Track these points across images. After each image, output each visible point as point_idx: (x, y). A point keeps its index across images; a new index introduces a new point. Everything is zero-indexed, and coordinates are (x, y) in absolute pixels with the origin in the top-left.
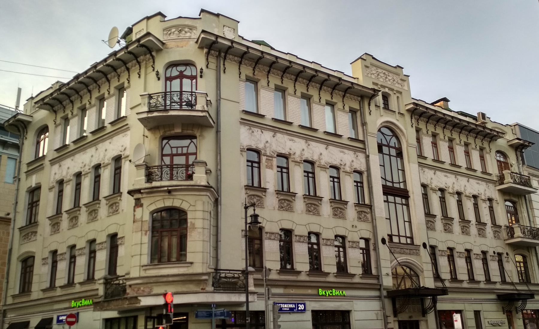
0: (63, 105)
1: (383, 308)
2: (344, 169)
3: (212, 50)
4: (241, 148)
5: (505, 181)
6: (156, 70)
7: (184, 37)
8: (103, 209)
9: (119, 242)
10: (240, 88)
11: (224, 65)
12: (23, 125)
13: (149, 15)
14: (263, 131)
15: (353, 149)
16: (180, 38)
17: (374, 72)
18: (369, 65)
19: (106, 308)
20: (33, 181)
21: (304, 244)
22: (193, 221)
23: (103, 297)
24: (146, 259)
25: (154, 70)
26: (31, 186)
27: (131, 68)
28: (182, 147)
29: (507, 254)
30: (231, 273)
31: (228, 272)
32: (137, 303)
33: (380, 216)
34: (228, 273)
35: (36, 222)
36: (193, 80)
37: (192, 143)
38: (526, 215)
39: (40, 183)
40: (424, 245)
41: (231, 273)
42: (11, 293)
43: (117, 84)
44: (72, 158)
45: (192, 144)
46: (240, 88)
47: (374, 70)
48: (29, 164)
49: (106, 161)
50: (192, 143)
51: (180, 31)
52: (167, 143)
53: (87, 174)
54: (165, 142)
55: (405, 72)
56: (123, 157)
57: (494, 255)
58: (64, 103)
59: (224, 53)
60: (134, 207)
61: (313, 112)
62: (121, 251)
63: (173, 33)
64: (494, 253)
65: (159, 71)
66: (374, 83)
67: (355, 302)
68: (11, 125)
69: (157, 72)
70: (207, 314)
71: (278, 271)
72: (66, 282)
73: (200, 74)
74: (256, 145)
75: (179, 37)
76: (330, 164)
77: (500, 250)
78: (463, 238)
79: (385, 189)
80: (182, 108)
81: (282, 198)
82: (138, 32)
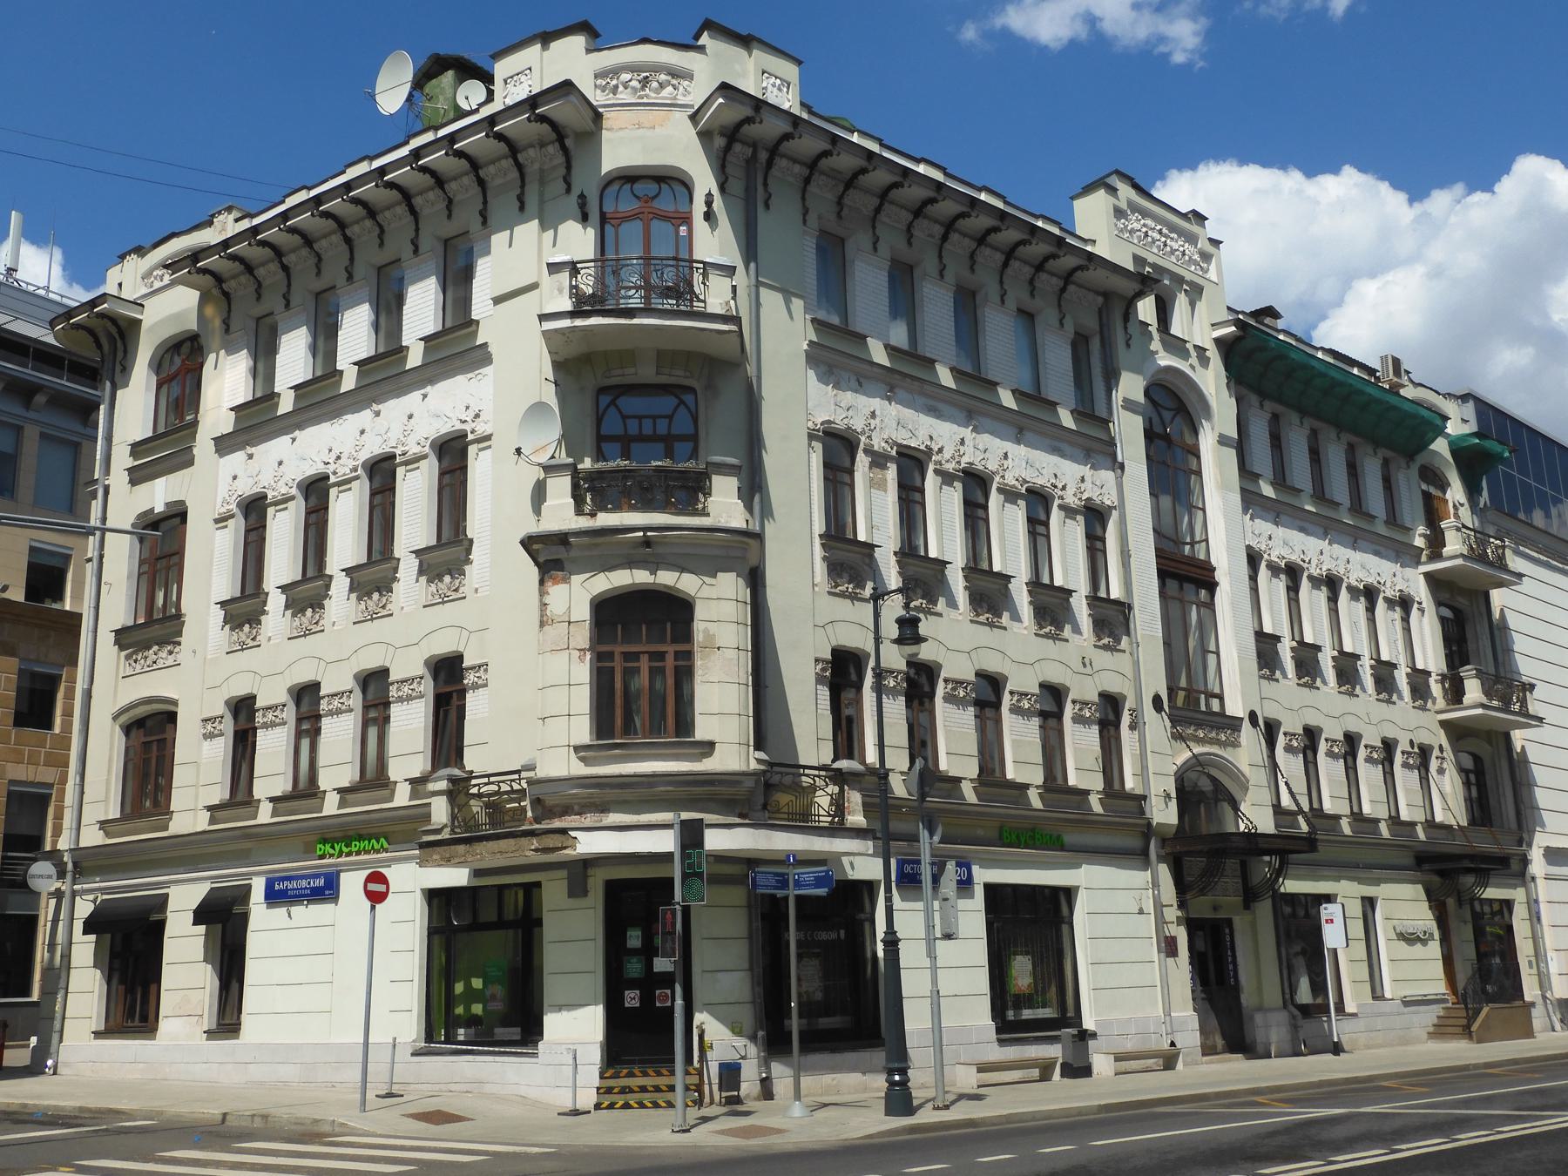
0: (255, 277)
1: (1155, 884)
2: (1061, 498)
5: (1445, 549)
6: (576, 192)
7: (656, 98)
8: (408, 584)
9: (470, 678)
10: (806, 253)
11: (765, 184)
12: (114, 330)
14: (861, 380)
16: (645, 100)
17: (1136, 226)
19: (462, 859)
20: (158, 494)
22: (712, 627)
23: (448, 830)
24: (582, 731)
25: (568, 190)
26: (152, 510)
28: (654, 418)
29: (1441, 749)
30: (493, 783)
31: (486, 780)
32: (565, 848)
33: (1148, 632)
34: (486, 784)
35: (167, 618)
36: (680, 225)
37: (682, 406)
38: (1488, 644)
39: (182, 503)
40: (1253, 717)
41: (493, 783)
42: (92, 814)
45: (682, 410)
46: (806, 253)
47: (1135, 223)
48: (137, 449)
49: (414, 449)
50: (682, 406)
51: (645, 82)
52: (613, 403)
53: (349, 481)
55: (1211, 229)
56: (470, 437)
57: (1410, 750)
59: (767, 150)
60: (542, 582)
61: (985, 330)
62: (475, 704)
64: (1411, 742)
66: (1137, 259)
68: (78, 329)
69: (582, 196)
70: (777, 881)
72: (289, 787)
74: (846, 421)
75: (641, 97)
76: (1028, 482)
77: (1423, 738)
78: (1342, 703)
79: (1163, 561)
80: (650, 304)
82: (512, 77)
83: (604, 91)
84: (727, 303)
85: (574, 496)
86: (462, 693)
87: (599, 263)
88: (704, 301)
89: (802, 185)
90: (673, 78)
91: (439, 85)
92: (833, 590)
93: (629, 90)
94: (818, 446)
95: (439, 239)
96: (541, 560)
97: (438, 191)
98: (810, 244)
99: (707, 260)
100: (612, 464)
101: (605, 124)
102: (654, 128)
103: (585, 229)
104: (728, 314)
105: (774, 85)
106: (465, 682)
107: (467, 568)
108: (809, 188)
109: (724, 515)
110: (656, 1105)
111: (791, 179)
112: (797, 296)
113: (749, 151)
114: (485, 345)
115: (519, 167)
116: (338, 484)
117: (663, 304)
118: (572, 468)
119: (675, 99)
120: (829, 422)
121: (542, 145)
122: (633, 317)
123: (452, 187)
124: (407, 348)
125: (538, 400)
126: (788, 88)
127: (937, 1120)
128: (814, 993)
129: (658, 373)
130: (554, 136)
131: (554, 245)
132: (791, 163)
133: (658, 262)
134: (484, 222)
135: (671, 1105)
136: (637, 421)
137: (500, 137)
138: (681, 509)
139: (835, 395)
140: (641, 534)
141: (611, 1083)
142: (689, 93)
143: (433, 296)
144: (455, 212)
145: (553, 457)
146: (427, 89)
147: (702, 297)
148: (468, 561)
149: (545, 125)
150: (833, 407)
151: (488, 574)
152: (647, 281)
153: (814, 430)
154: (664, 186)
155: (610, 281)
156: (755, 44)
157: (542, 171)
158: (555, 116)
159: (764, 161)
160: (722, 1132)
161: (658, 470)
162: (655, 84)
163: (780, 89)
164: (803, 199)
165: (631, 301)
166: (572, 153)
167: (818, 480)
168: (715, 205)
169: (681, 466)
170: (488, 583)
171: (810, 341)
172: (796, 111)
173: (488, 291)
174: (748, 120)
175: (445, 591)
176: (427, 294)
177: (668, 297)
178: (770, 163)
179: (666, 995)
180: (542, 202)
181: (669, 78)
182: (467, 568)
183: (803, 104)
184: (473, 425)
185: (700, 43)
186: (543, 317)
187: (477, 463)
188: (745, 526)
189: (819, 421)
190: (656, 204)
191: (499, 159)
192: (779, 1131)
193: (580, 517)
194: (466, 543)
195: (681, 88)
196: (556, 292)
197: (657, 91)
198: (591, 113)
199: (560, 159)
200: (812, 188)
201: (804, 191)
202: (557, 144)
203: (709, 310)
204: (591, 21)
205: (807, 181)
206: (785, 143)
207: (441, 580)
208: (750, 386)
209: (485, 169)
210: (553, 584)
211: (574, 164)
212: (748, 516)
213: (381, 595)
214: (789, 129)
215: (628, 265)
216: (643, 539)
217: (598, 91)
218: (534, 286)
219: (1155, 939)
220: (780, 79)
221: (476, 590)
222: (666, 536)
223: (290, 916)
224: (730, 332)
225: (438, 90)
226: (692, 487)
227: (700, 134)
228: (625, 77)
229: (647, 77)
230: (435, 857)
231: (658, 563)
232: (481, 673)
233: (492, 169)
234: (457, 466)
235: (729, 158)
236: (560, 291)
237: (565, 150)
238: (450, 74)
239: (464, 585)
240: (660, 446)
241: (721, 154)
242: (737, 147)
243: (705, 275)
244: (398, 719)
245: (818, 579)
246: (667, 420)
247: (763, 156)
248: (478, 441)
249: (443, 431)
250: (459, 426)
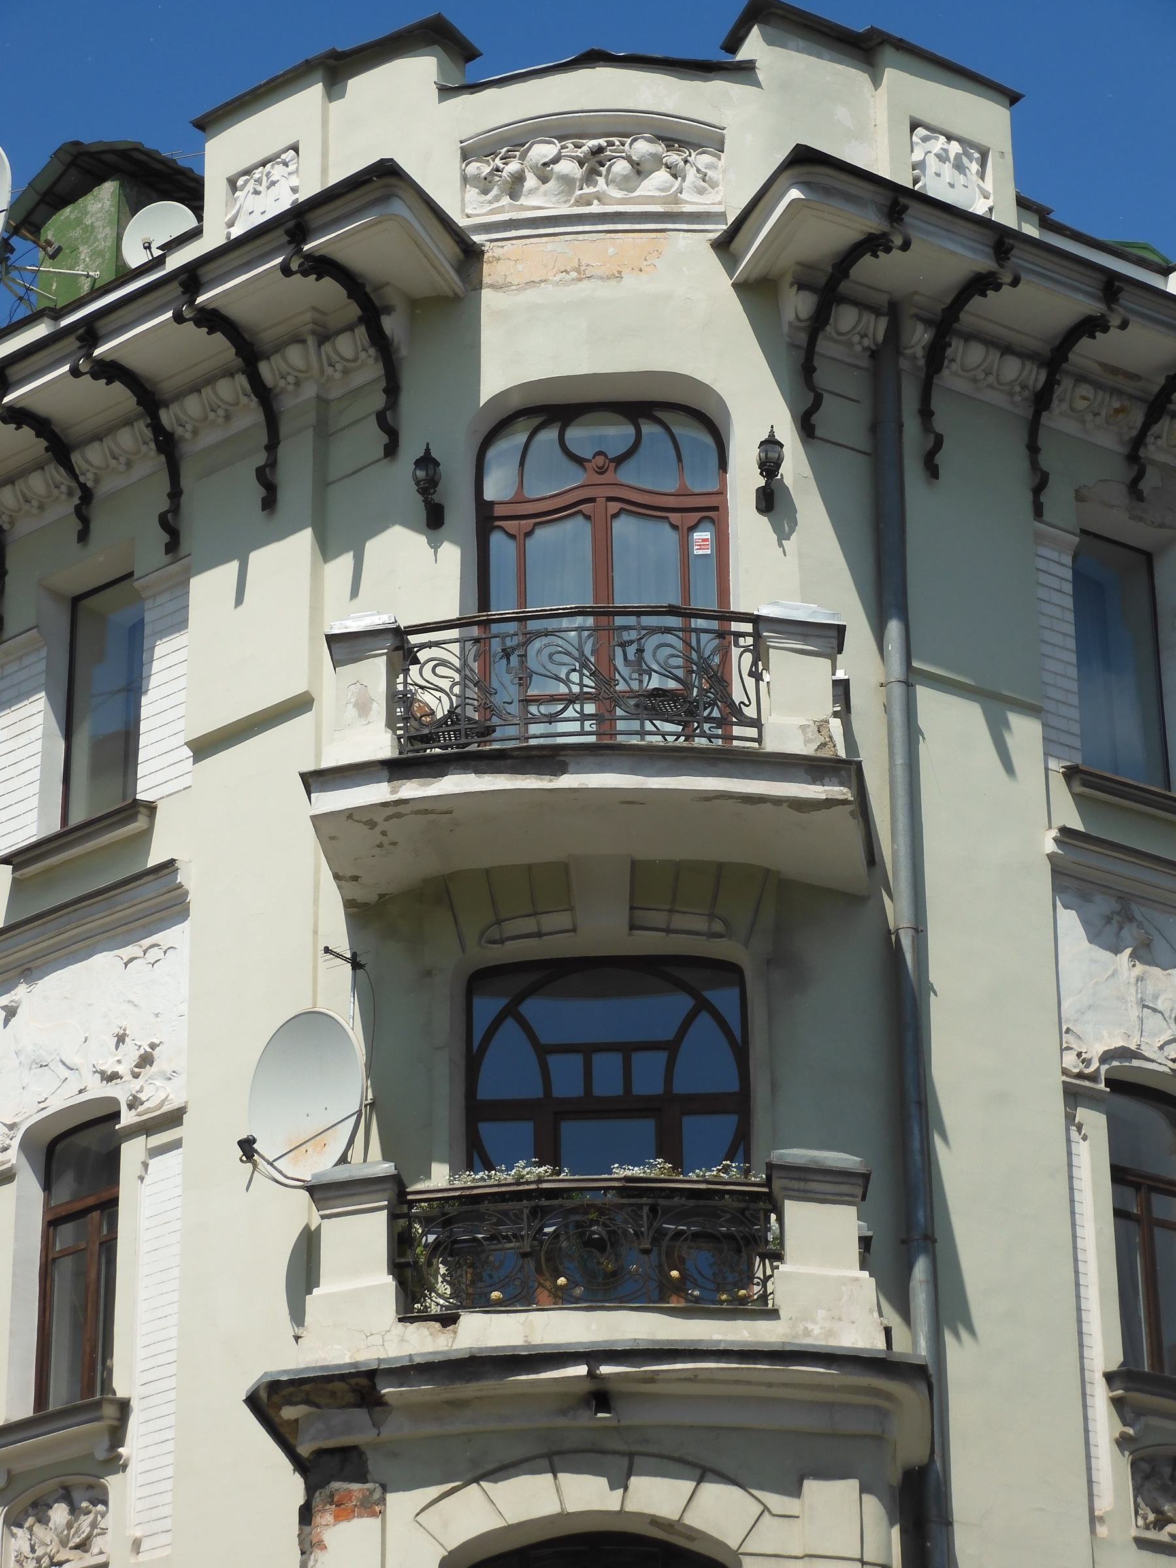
3: (844, 300)
4: (1065, 1072)
6: (411, 450)
11: (926, 413)
13: (344, 45)
16: (596, 208)
25: (391, 449)
28: (627, 1049)
36: (693, 528)
51: (595, 162)
52: (510, 1011)
54: (487, 1007)
56: (127, 1118)
59: (928, 322)
60: (306, 1515)
63: (544, 172)
65: (434, 454)
69: (427, 461)
73: (762, 482)
82: (248, 172)
83: (485, 192)
84: (821, 726)
85: (398, 1267)
87: (475, 631)
88: (757, 723)
89: (1029, 413)
90: (669, 147)
91: (79, 221)
92: (1151, 1535)
93: (552, 184)
94: (1094, 1121)
95: (55, 595)
96: (304, 1450)
97: (56, 473)
98: (1055, 569)
99: (765, 611)
100: (501, 1177)
101: (490, 273)
102: (619, 276)
103: (435, 545)
104: (826, 753)
105: (942, 157)
107: (112, 1482)
108: (1045, 419)
109: (821, 1314)
111: (997, 398)
112: (1032, 710)
113: (881, 326)
114: (169, 865)
115: (264, 395)
117: (643, 733)
118: (391, 1190)
119: (677, 201)
120: (1124, 1053)
121: (324, 336)
122: (560, 769)
123: (89, 459)
125: (306, 1006)
126: (983, 164)
129: (633, 927)
130: (354, 310)
131: (355, 593)
132: (995, 355)
133: (631, 620)
134: (173, 546)
136: (577, 1060)
137: (211, 319)
138: (697, 1300)
139: (1140, 979)
140: (582, 1370)
142: (714, 185)
143: (38, 746)
144: (97, 527)
145: (343, 1160)
146: (49, 233)
147: (750, 712)
148: (115, 1464)
149: (328, 281)
150: (1134, 1012)
151: (168, 1498)
152: (605, 680)
153: (1080, 1076)
154: (649, 429)
155: (506, 690)
156: (888, 53)
157: (322, 401)
158: (354, 257)
159: (920, 353)
161: (631, 1189)
162: (621, 167)
163: (959, 167)
164: (1033, 449)
165: (562, 727)
166: (404, 352)
167: (1096, 1216)
168: (788, 472)
169: (696, 1177)
170: (167, 1524)
171: (1064, 830)
172: (1008, 216)
173: (181, 725)
174: (873, 244)
175: (52, 1549)
176: (23, 740)
177: (655, 714)
178: (936, 357)
180: (322, 484)
181: (660, 148)
182: (112, 1482)
183: (1023, 203)
184: (136, 1085)
185: (743, 55)
186: (315, 780)
187: (145, 1189)
188: (881, 1344)
189: (1095, 1050)
190: (627, 475)
191: (210, 380)
193: (412, 1328)
194: (109, 1411)
195: (691, 173)
196: (351, 712)
197: (625, 183)
198: (452, 249)
199: (371, 370)
200: (1056, 420)
201: (1034, 428)
202: (361, 331)
203: (772, 745)
205: (1042, 400)
206: (976, 302)
207: (43, 1520)
208: (896, 952)
209: (175, 408)
210: (338, 1518)
212: (893, 1318)
213: (74, 1510)
214: (983, 262)
215: (547, 634)
216: (588, 1386)
217: (472, 193)
218: (300, 705)
220: (960, 140)
221: (137, 1545)
222: (652, 1378)
224: (829, 803)
225: (77, 232)
226: (730, 1237)
227: (741, 287)
228: (542, 151)
229: (600, 150)
231: (631, 1455)
233: (192, 406)
234: (90, 1201)
235: (823, 346)
236: (363, 708)
237: (381, 343)
238: (108, 191)
239: (104, 1531)
240: (645, 1128)
241: (803, 338)
242: (846, 318)
243: (759, 653)
245: (1104, 1504)
246: (662, 1057)
247: (919, 337)
248: (147, 1128)
249: (57, 1104)
250: (98, 1090)
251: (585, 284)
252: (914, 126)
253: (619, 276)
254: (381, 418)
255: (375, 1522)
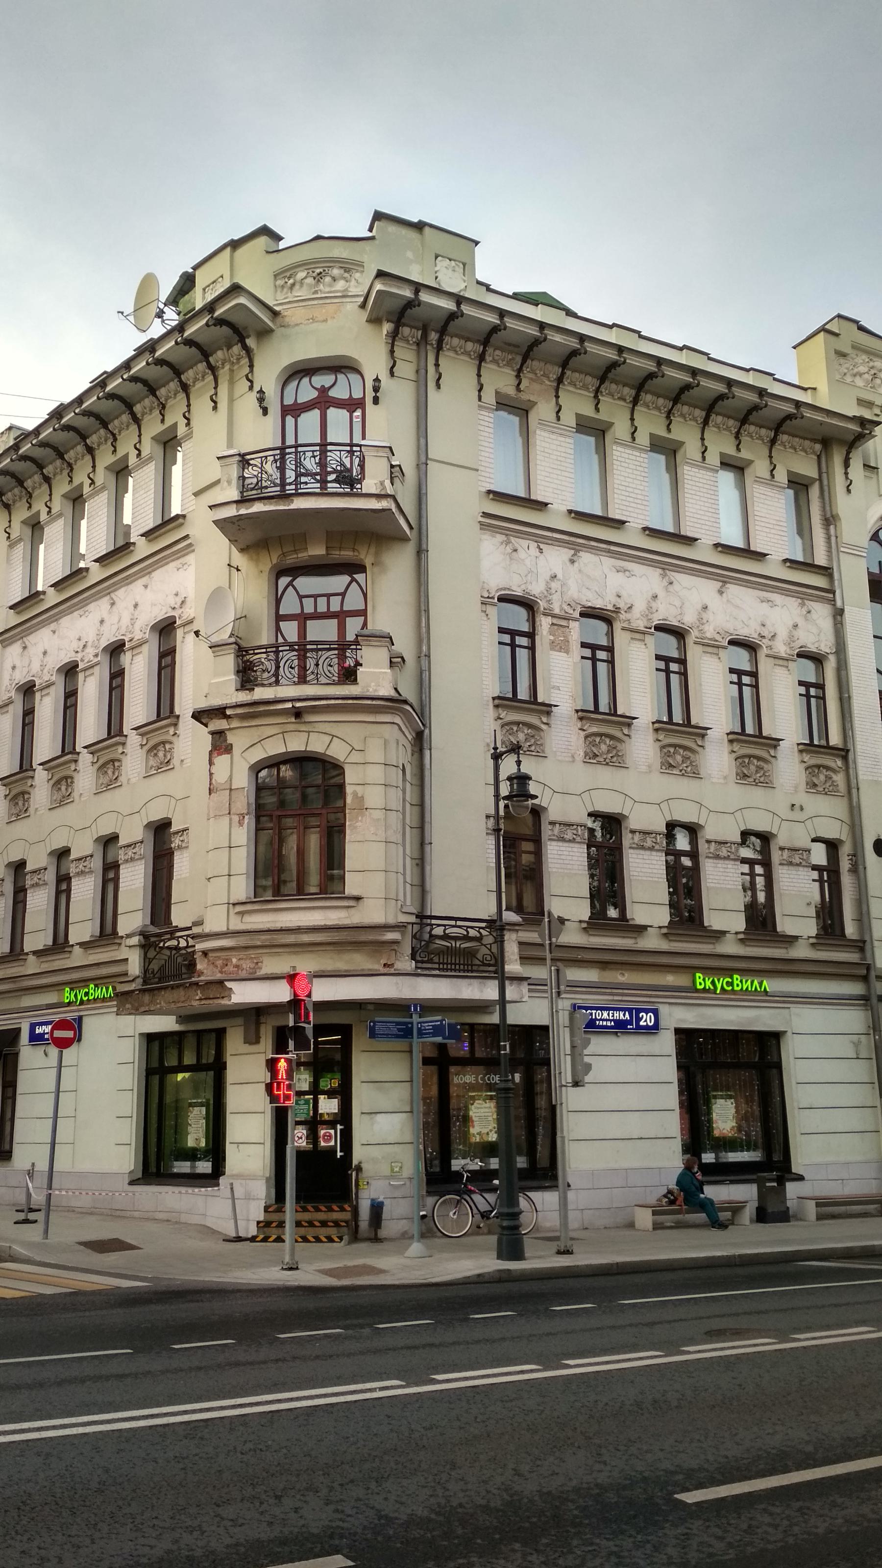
2: (770, 647)
6: (257, 388)
7: (329, 292)
9: (176, 842)
11: (437, 365)
14: (542, 546)
15: (797, 592)
18: (847, 350)
19: (147, 1009)
21: (654, 853)
23: (140, 981)
24: (242, 888)
25: (251, 388)
27: (194, 386)
28: (328, 596)
30: (460, 927)
36: (354, 411)
37: (354, 583)
41: (460, 927)
43: (159, 428)
44: (53, 626)
49: (138, 636)
51: (319, 277)
52: (290, 584)
54: (284, 581)
58: (29, 483)
59: (436, 331)
60: (211, 753)
62: (182, 865)
67: (796, 1009)
69: (261, 392)
70: (399, 1030)
71: (584, 925)
75: (316, 292)
76: (731, 635)
81: (594, 729)
82: (209, 286)
86: (171, 854)
106: (173, 845)
109: (373, 684)
110: (318, 1240)
116: (85, 670)
124: (134, 544)
127: (558, 1265)
128: (488, 1134)
135: (279, 1240)
141: (306, 1216)
149: (224, 327)
154: (341, 377)
159: (434, 342)
160: (320, 1271)
166: (255, 351)
179: (330, 1136)
192: (381, 1271)
204: (271, 226)
211: (256, 363)
219: (877, 1084)
223: (46, 1055)
229: (321, 273)
230: (128, 1006)
232: (184, 837)
244: (125, 880)
251: (315, 324)
252: (436, 257)
253: (326, 321)
254: (247, 376)
255: (229, 756)
